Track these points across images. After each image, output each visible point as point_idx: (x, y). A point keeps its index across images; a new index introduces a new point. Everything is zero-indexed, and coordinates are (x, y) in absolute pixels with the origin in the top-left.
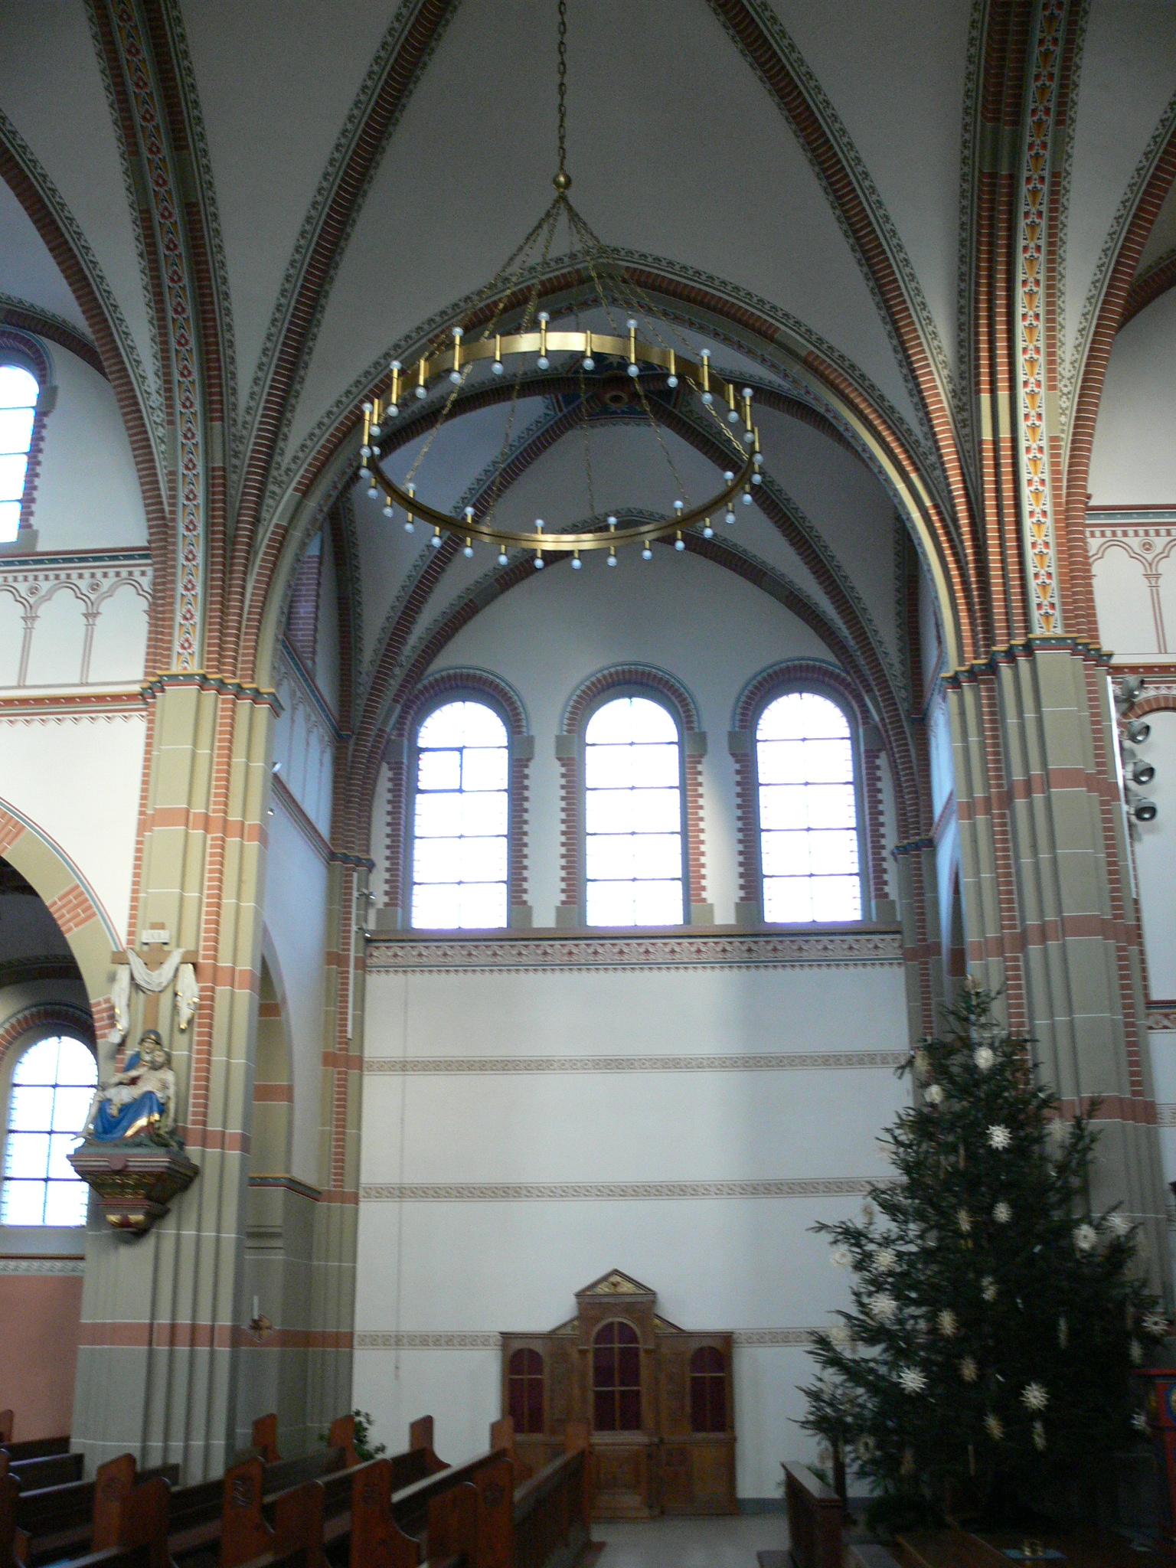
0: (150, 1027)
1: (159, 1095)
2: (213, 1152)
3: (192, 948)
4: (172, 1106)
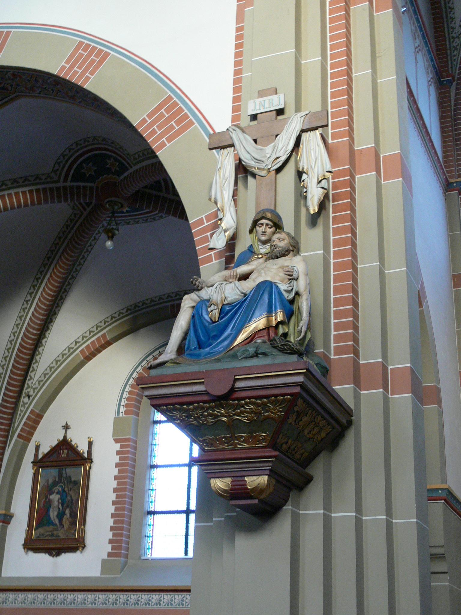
0: (266, 204)
1: (283, 287)
2: (371, 395)
3: (319, 108)
4: (304, 304)
